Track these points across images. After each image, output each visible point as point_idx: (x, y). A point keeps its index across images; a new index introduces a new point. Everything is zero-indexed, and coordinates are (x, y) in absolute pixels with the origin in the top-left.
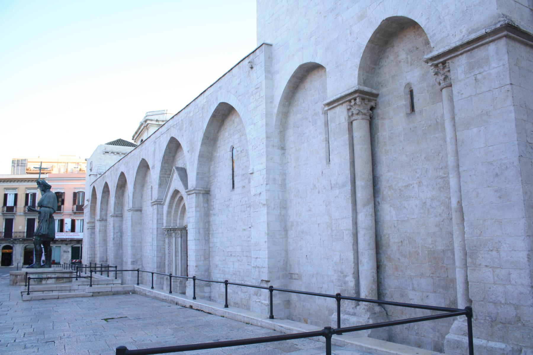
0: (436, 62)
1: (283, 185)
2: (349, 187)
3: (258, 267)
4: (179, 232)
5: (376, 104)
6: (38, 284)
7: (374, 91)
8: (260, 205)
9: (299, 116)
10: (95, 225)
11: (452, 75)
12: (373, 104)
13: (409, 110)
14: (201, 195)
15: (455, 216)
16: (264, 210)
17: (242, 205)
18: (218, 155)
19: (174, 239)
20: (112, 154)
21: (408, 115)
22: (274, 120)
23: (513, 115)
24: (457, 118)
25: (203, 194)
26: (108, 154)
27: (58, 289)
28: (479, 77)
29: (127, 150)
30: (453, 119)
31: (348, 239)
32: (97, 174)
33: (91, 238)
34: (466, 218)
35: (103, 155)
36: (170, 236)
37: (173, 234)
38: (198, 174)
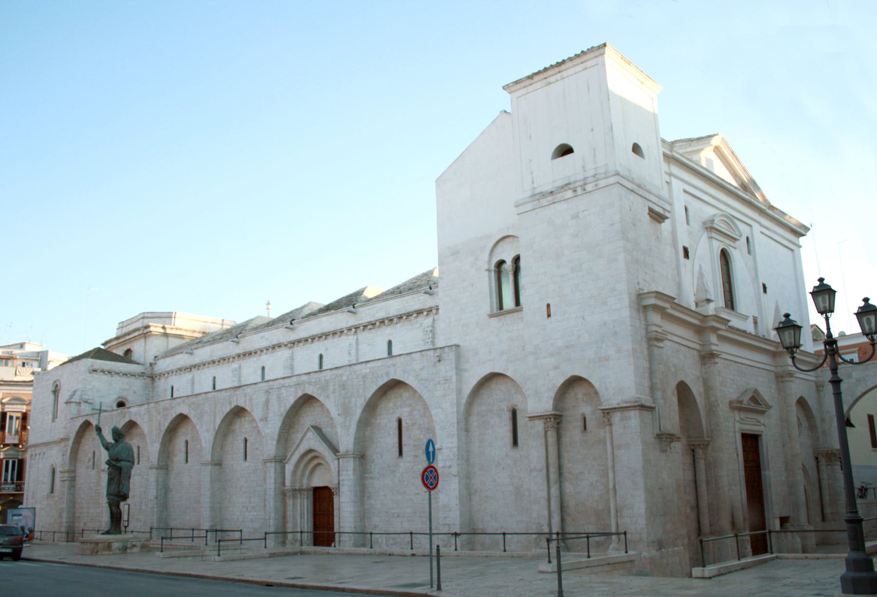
0: (604, 411)
1: (468, 460)
2: (545, 472)
3: (448, 525)
4: (306, 493)
5: (561, 421)
6: (122, 553)
7: (561, 414)
8: (451, 475)
9: (483, 408)
10: (75, 475)
11: (612, 420)
12: (559, 421)
13: (583, 429)
14: (357, 459)
15: (611, 492)
16: (456, 480)
17: (413, 472)
18: (378, 422)
19: (299, 500)
20: (102, 374)
21: (582, 432)
22: (462, 407)
23: (640, 447)
24: (614, 443)
25: (359, 458)
26: (95, 372)
27: (192, 555)
28: (626, 425)
29: (121, 368)
30: (612, 442)
31: (544, 503)
32: (81, 401)
33: (69, 493)
34: (617, 493)
35: (88, 375)
36: (294, 497)
37: (298, 495)
38: (355, 438)
